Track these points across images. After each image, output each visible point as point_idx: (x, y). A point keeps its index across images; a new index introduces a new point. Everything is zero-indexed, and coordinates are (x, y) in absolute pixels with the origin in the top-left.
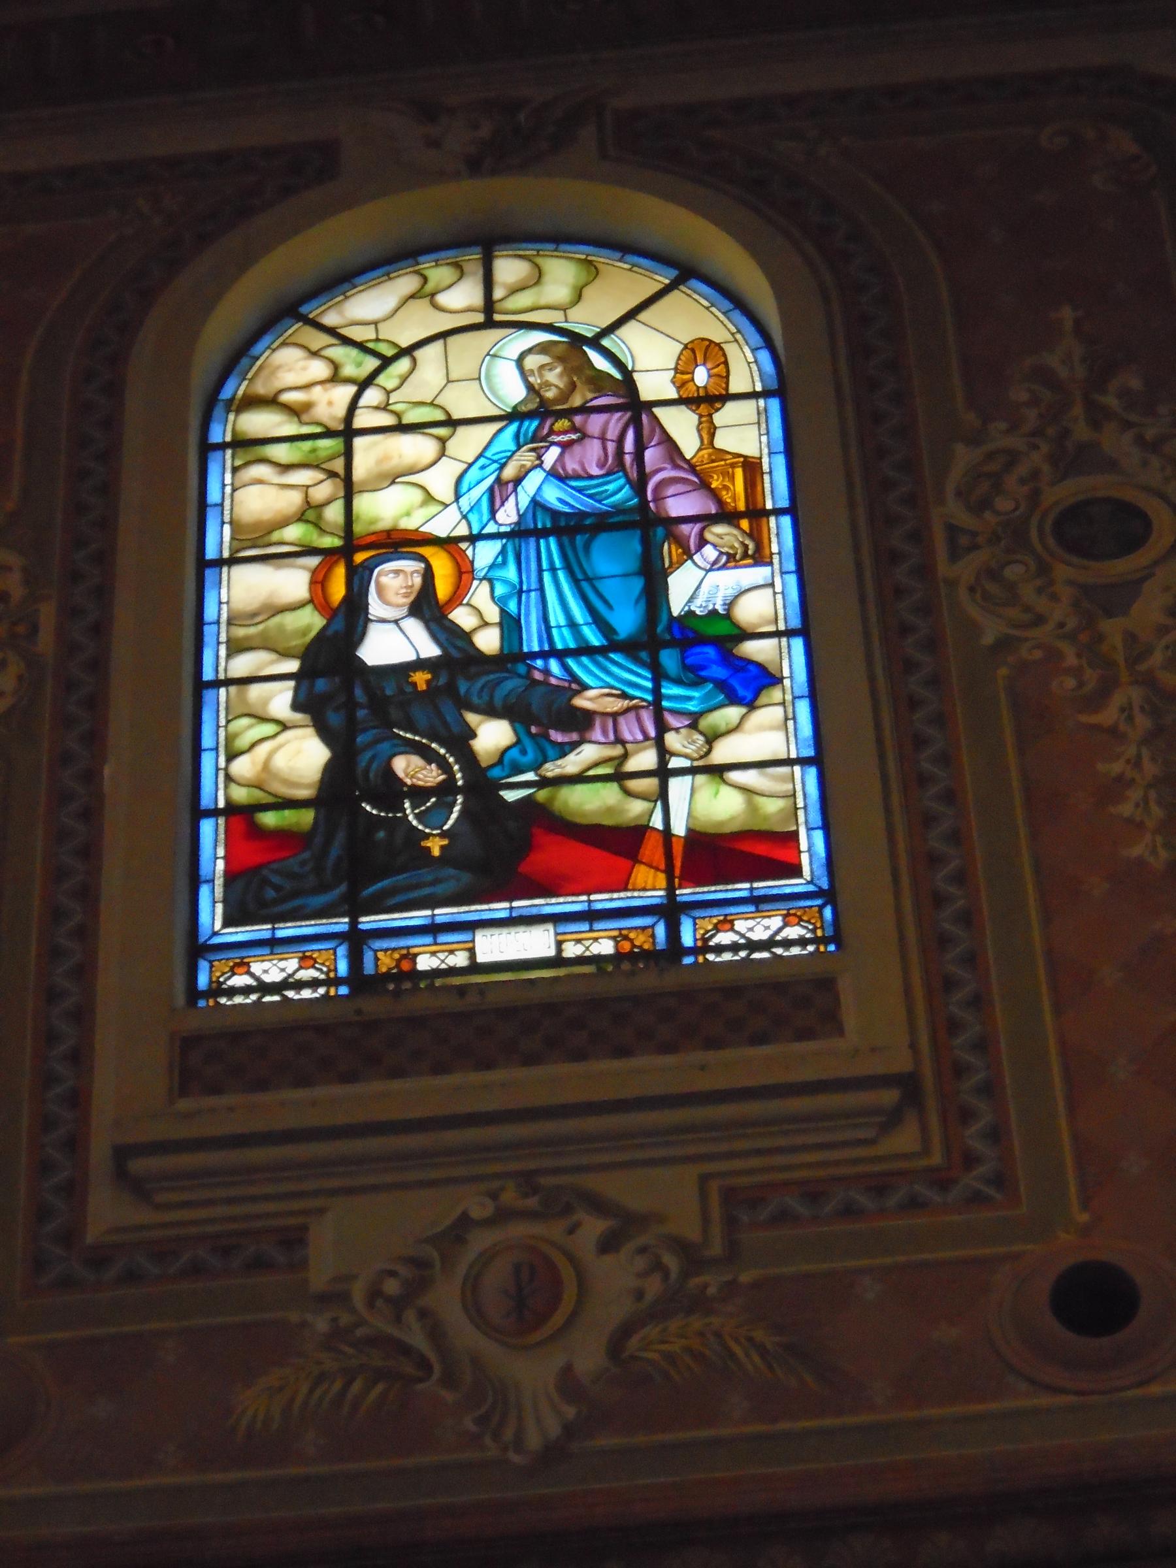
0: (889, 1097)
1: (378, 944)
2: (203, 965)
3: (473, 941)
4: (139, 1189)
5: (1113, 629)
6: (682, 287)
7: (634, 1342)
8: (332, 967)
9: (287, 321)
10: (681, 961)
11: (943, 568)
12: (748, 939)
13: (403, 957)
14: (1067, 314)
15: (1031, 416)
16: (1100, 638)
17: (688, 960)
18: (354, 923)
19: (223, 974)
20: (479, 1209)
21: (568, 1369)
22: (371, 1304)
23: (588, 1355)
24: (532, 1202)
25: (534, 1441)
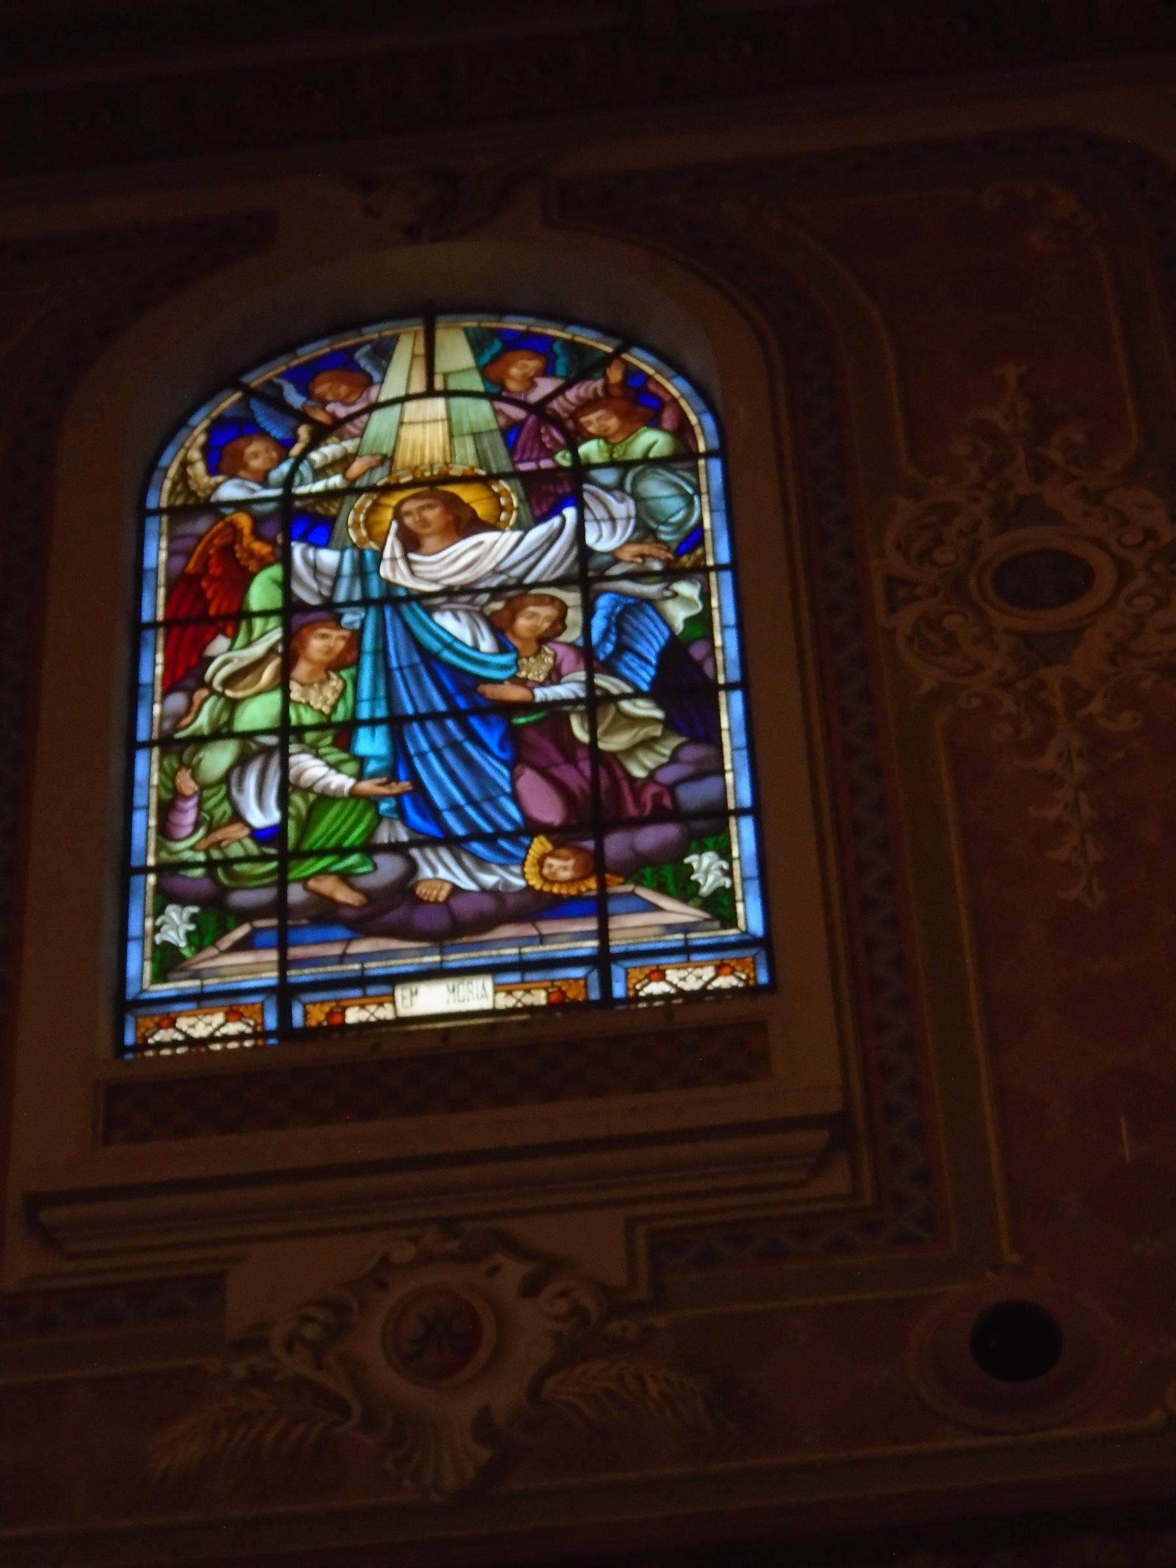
0: (818, 1138)
1: (306, 998)
5: (1053, 675)
7: (551, 1383)
8: (752, 975)
14: (1011, 372)
16: (1041, 685)
19: (639, 981)
20: (404, 1253)
21: (486, 1410)
22: (289, 1346)
24: (453, 1246)
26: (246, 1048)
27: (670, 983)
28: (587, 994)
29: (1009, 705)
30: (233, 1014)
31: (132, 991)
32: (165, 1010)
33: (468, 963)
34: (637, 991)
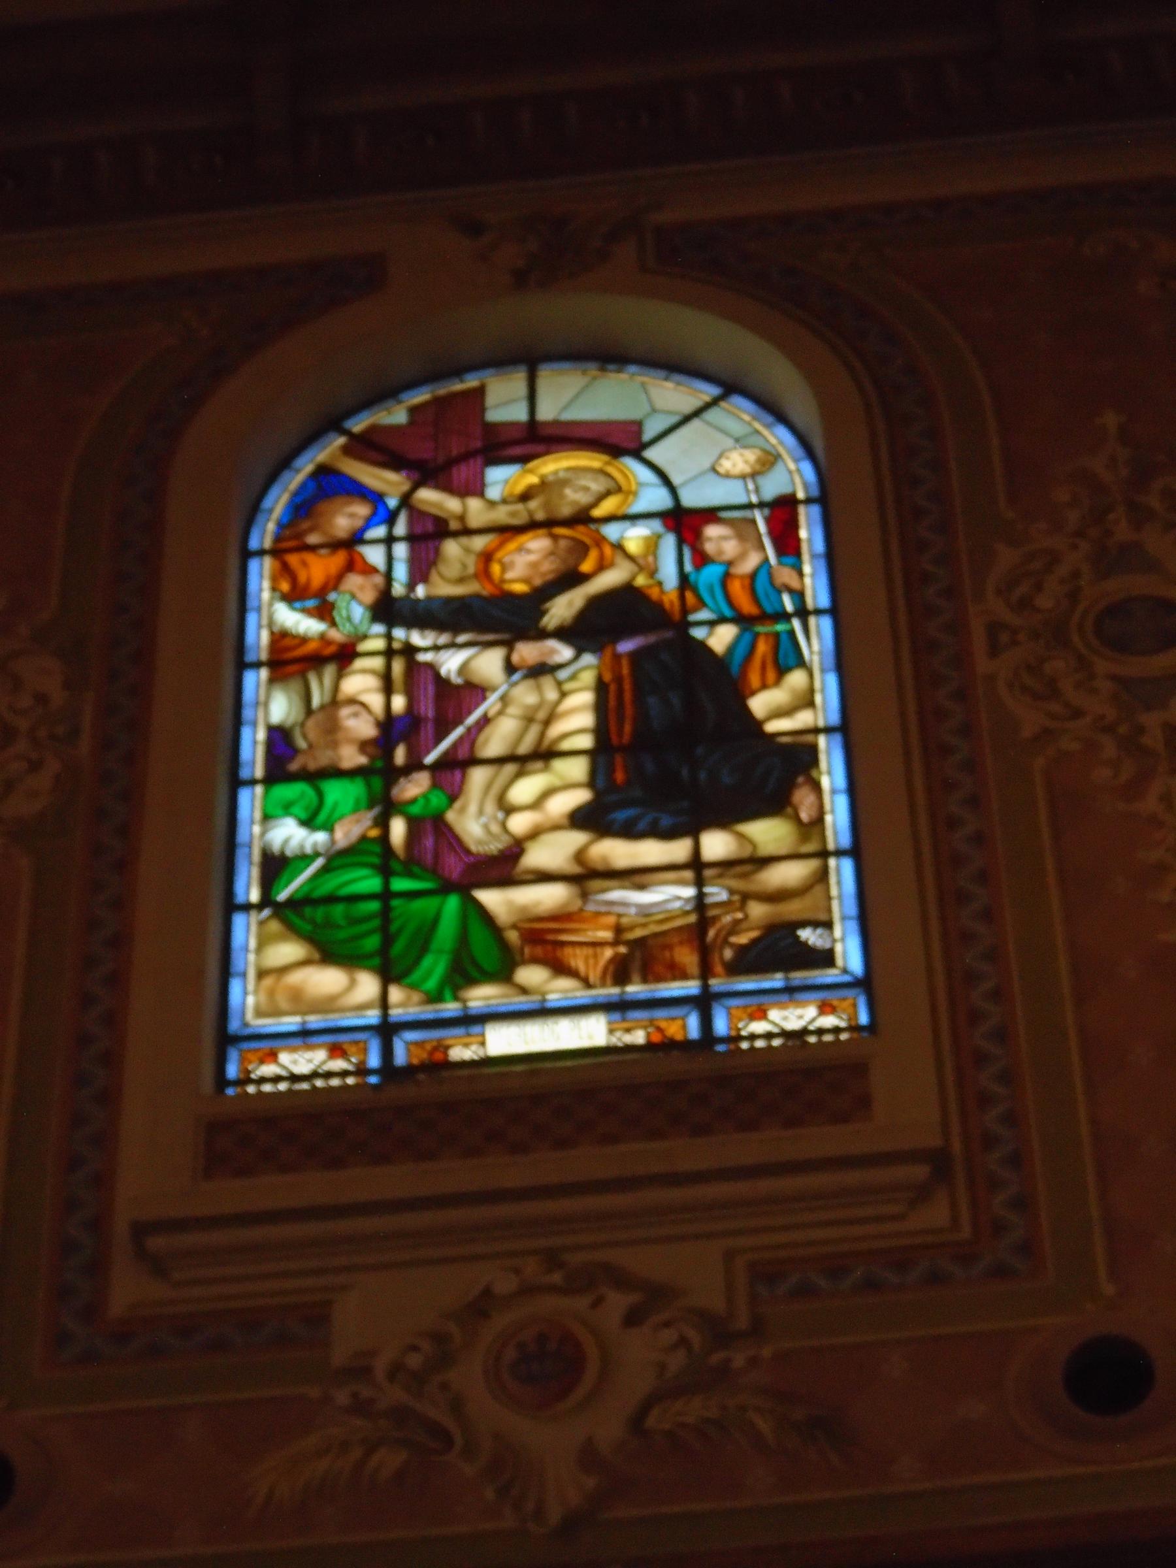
0: (920, 1172)
2: (233, 1056)
4: (158, 1267)
5: (1152, 720)
11: (983, 664)
13: (435, 1049)
14: (1111, 420)
16: (1141, 730)
17: (721, 1048)
20: (505, 1285)
23: (607, 1426)
24: (557, 1278)
25: (555, 1515)
26: (348, 1086)
29: (1109, 748)
30: (336, 1051)
31: (234, 1026)
34: (739, 1030)
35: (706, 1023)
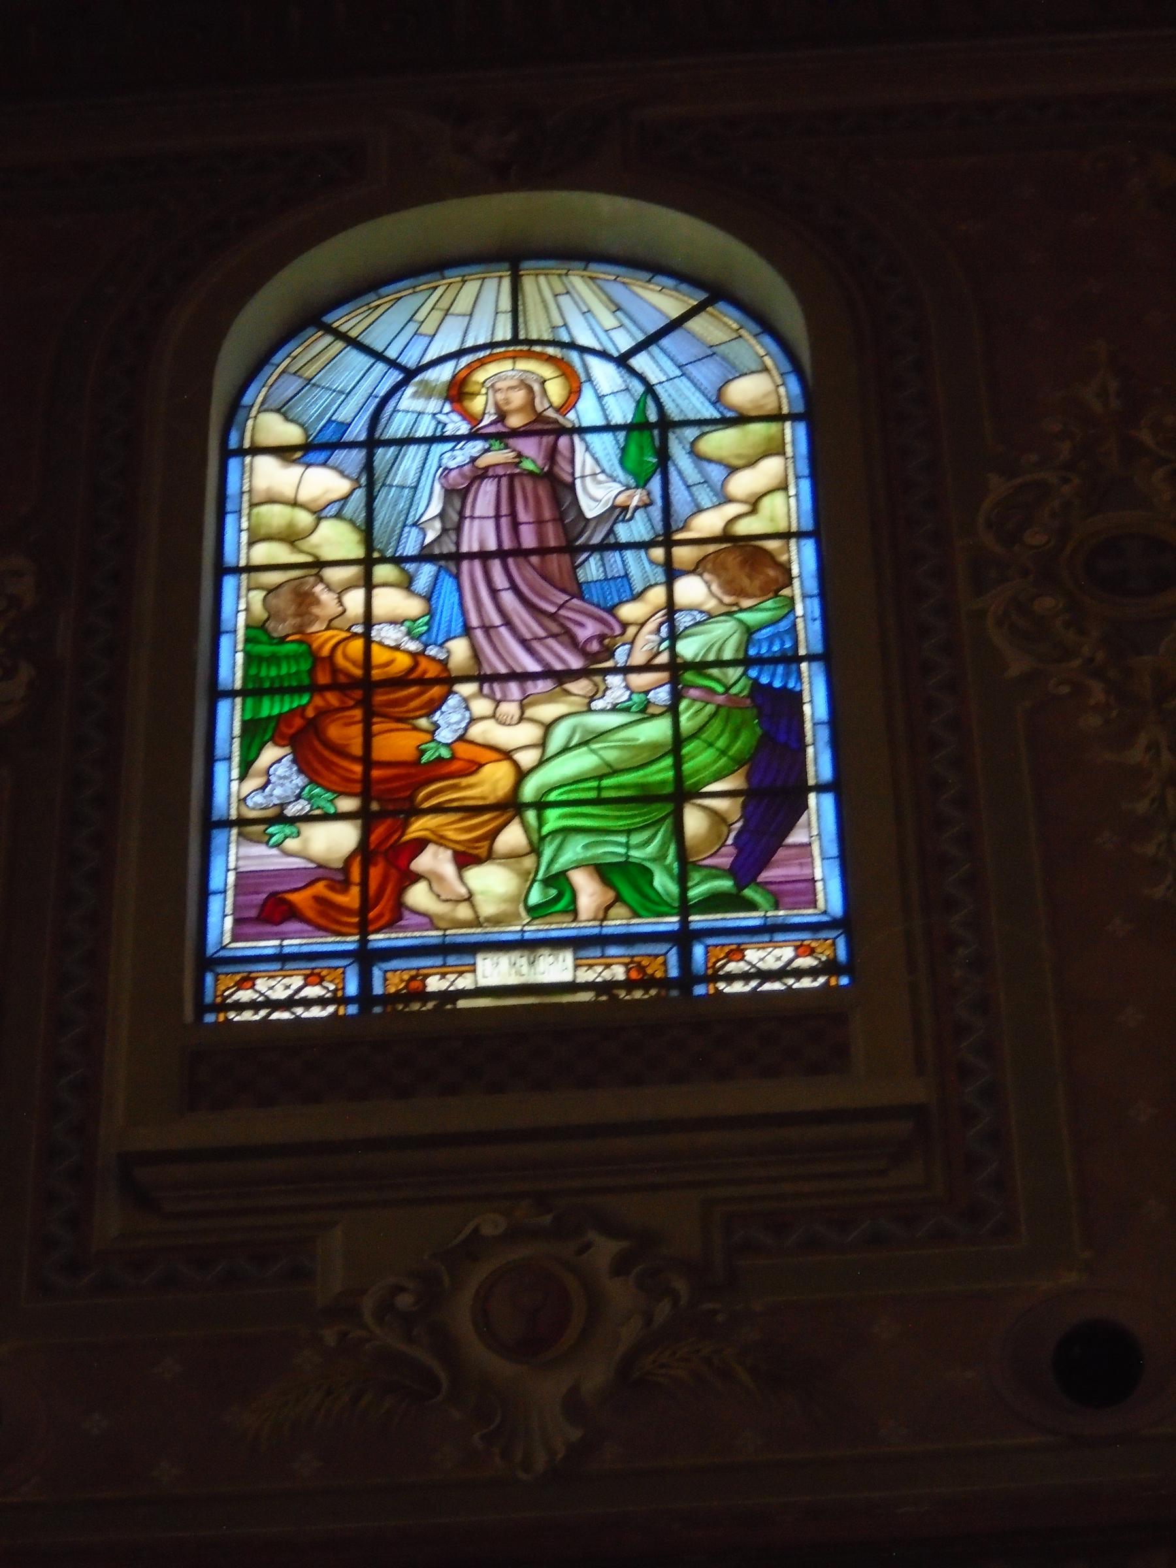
3: (474, 964)
6: (542, 279)
9: (310, 331)
10: (370, 1011)
12: (758, 969)
13: (413, 978)
15: (1065, 448)
18: (364, 941)
20: (491, 1225)
21: (575, 1389)
23: (595, 1376)
25: (541, 1462)
27: (749, 963)
28: (666, 971)
29: (1098, 692)
30: (802, 949)
31: (211, 949)
32: (247, 968)
33: (305, 949)
35: (685, 958)
